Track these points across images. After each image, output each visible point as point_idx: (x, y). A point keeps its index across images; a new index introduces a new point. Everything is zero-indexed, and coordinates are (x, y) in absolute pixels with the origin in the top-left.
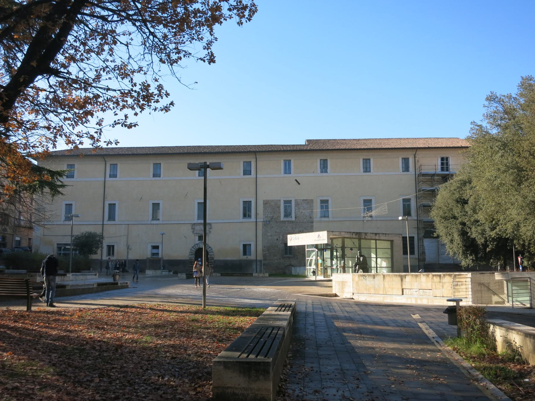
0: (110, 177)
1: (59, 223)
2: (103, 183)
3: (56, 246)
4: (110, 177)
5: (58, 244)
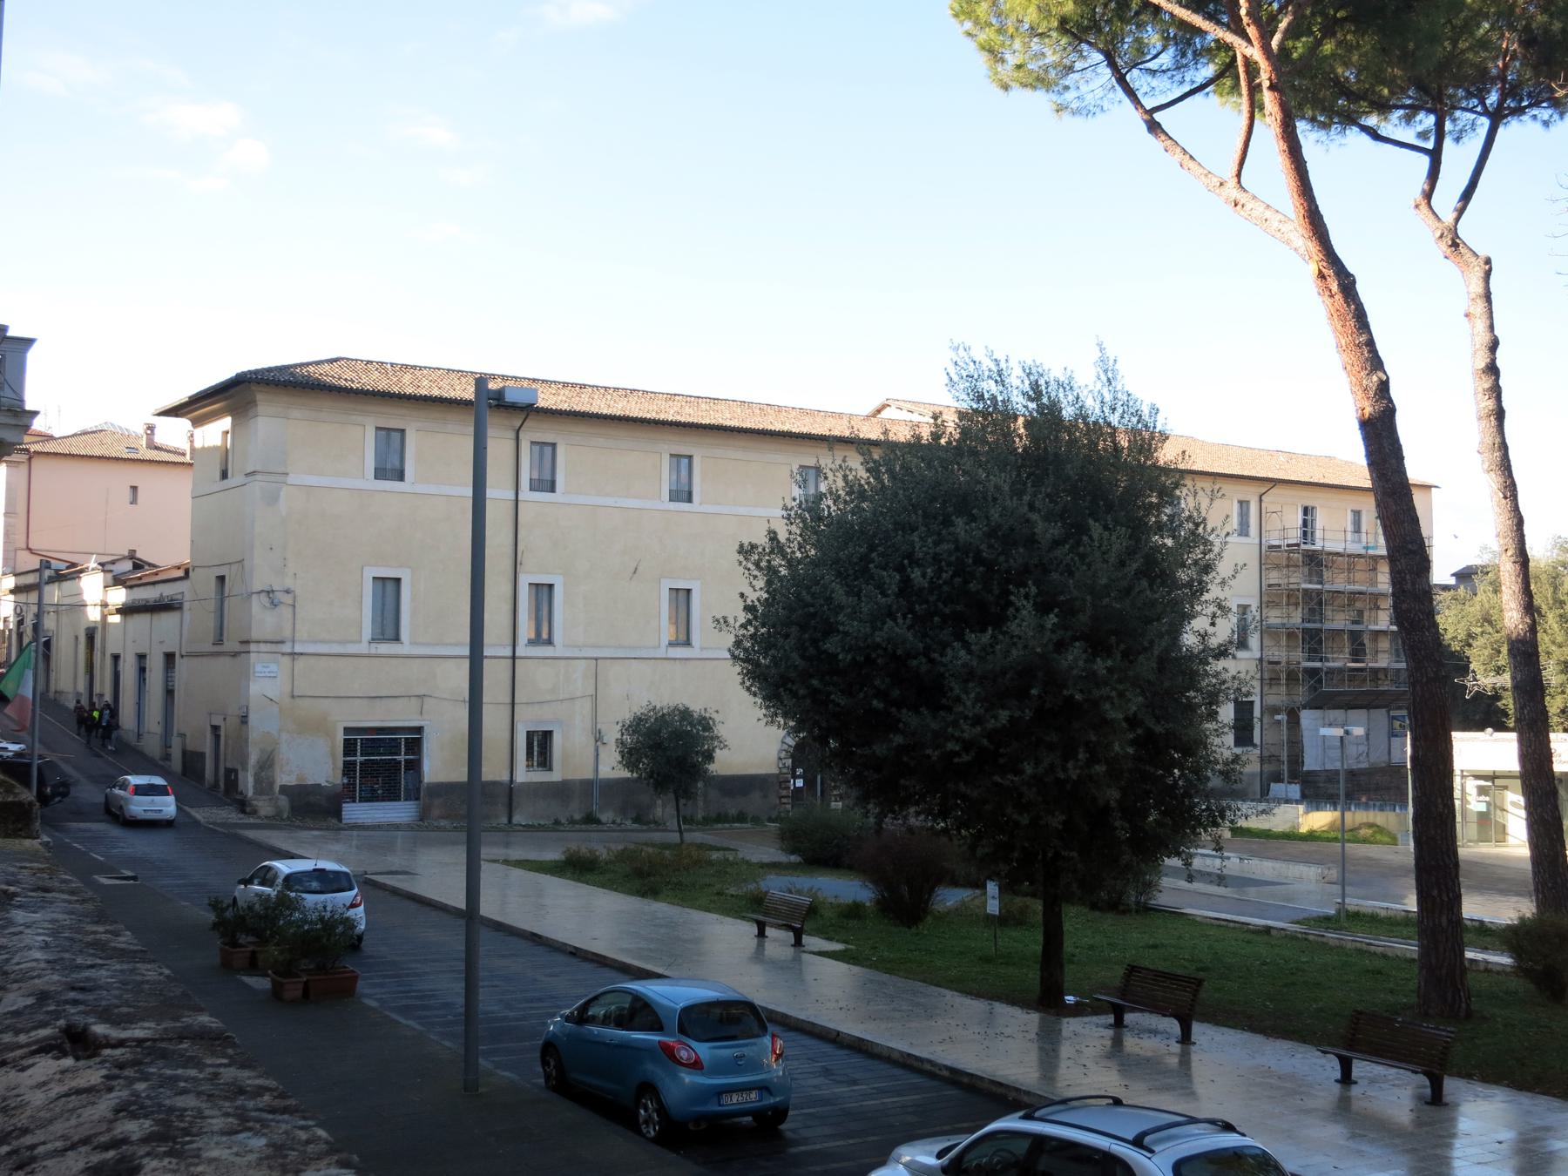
2: (511, 505)
3: (340, 737)
5: (347, 730)
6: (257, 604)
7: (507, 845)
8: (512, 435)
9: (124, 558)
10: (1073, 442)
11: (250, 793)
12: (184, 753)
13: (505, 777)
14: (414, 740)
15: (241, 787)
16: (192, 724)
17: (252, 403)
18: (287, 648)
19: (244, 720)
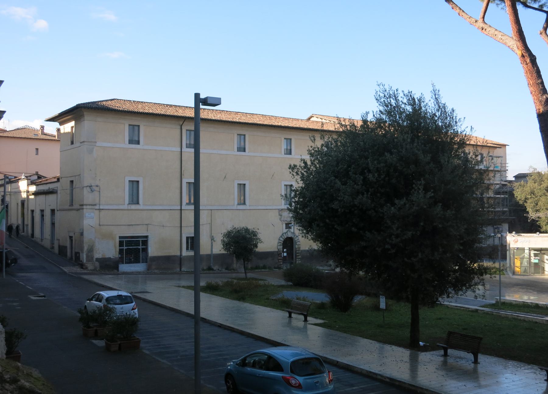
1: (121, 207)
3: (118, 240)
5: (120, 237)
6: (86, 191)
7: (179, 279)
8: (179, 127)
9: (34, 174)
11: (85, 261)
12: (59, 246)
13: (179, 254)
14: (145, 241)
15: (81, 259)
16: (62, 235)
17: (83, 116)
18: (97, 207)
19: (82, 234)
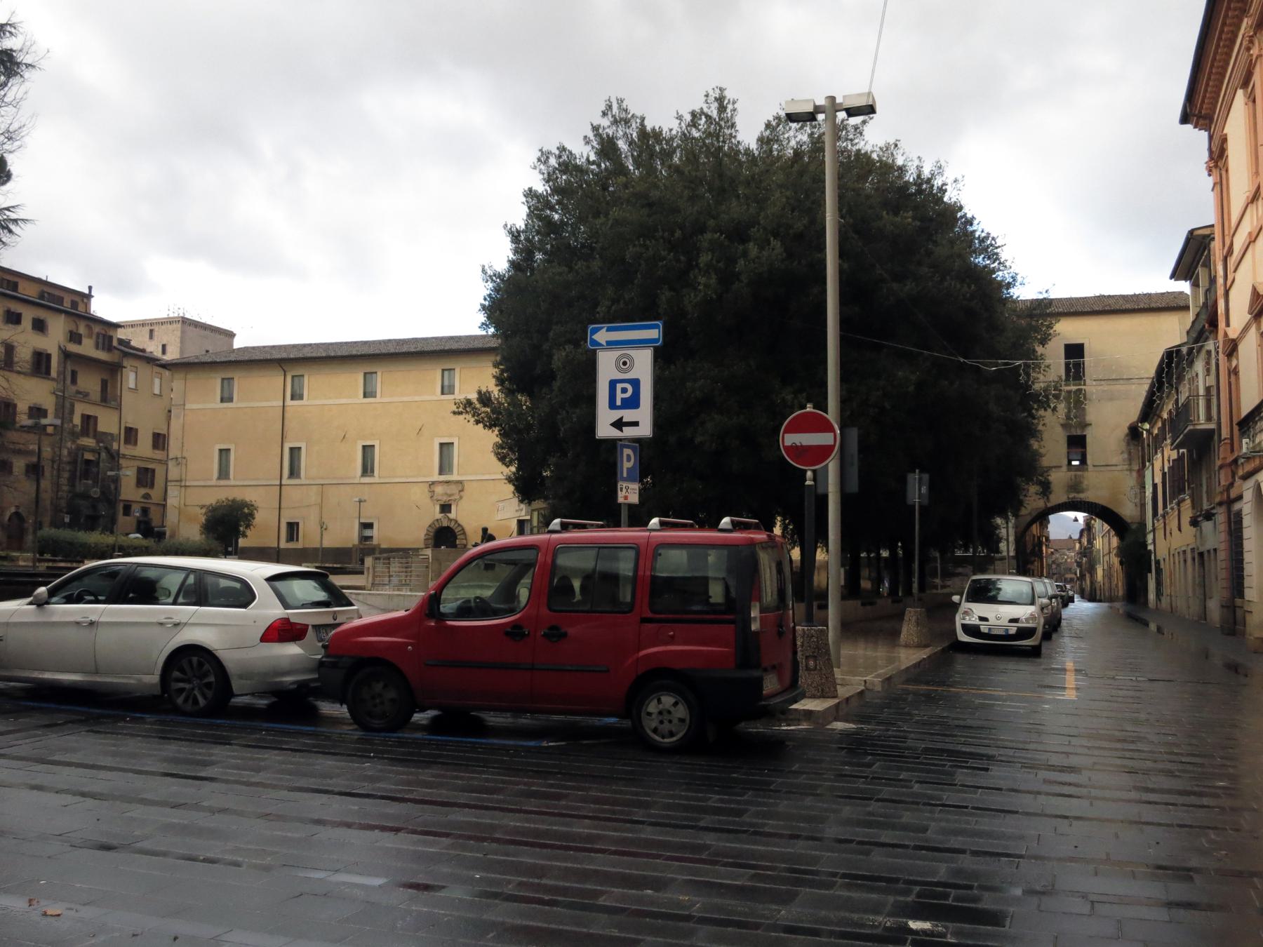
0: (292, 399)
4: (292, 399)
10: (502, 371)
